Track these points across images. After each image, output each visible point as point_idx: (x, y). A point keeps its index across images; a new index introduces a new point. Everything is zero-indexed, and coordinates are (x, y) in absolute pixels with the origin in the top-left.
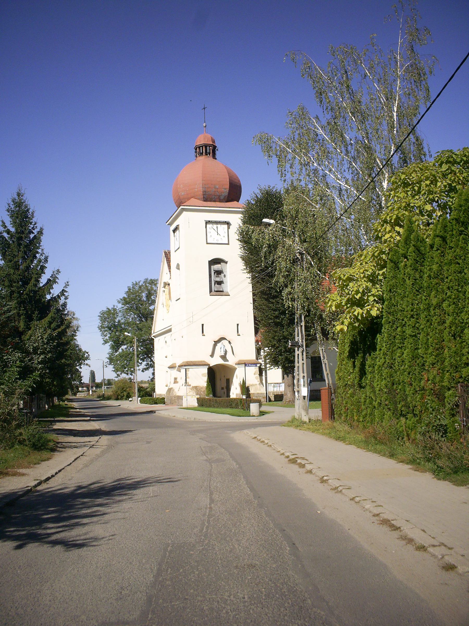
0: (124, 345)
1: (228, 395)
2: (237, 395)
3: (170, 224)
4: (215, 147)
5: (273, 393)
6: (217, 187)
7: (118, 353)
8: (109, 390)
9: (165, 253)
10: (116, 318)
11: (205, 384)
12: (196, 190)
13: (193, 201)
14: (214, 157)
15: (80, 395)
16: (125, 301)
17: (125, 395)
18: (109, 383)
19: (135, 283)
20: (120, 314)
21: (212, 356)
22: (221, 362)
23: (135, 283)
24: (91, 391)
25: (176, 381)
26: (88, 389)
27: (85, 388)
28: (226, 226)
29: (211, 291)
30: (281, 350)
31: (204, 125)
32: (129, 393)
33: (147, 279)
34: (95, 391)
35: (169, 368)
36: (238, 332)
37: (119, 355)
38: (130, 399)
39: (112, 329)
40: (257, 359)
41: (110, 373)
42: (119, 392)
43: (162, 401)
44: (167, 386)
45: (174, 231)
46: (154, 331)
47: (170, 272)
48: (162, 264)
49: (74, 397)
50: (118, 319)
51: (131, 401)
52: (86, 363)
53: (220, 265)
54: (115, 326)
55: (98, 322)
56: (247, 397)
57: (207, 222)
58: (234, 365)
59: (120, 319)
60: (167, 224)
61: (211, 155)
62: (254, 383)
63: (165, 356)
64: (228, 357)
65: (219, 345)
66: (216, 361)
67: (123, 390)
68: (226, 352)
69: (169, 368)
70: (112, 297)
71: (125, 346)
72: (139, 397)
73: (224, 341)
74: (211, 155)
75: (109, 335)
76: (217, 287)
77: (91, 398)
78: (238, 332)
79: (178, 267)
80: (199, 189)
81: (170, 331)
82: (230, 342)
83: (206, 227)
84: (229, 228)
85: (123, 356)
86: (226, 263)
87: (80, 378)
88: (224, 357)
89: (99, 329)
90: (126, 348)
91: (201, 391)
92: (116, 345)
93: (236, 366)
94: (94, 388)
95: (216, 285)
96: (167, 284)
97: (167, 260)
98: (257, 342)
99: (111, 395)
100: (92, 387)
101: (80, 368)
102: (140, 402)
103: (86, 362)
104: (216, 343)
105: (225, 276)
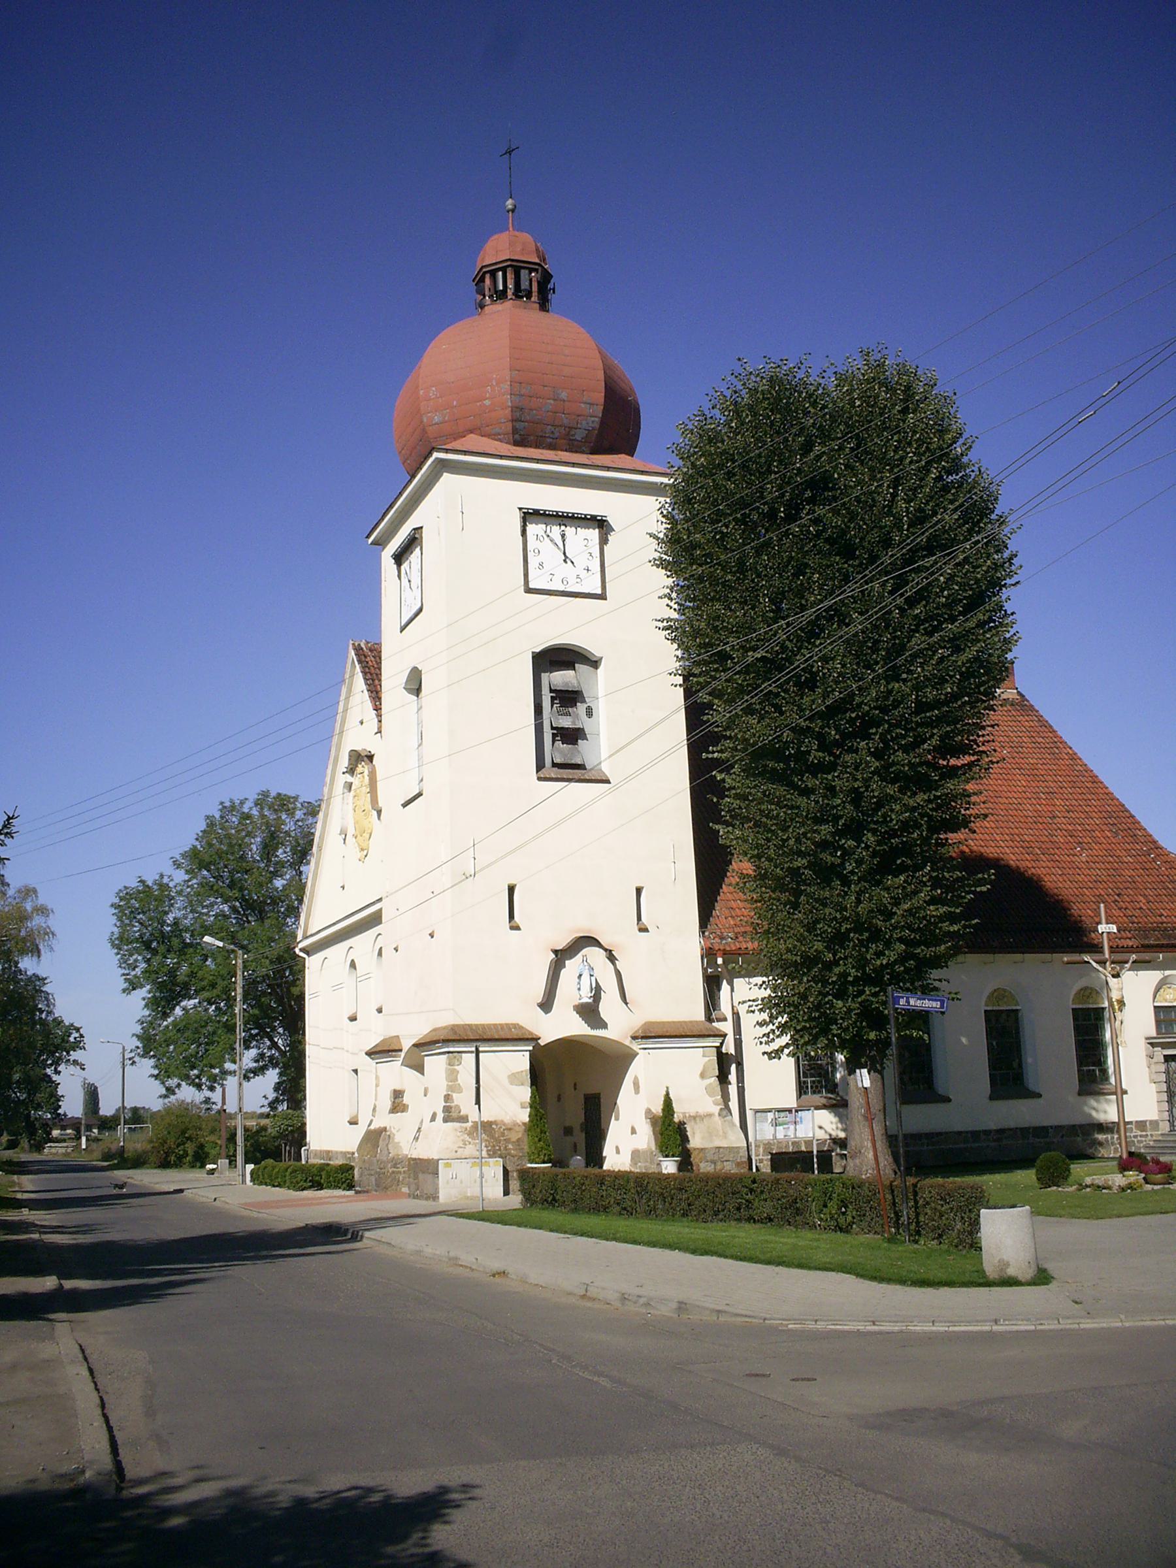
0: (190, 998)
1: (595, 1156)
2: (636, 1154)
3: (381, 543)
4: (546, 277)
5: (768, 1145)
6: (564, 395)
7: (170, 1020)
8: (136, 1136)
9: (358, 650)
10: (166, 913)
11: (524, 1116)
12: (487, 402)
13: (473, 441)
14: (544, 305)
15: (53, 1150)
16: (196, 860)
17: (190, 1152)
18: (137, 1116)
19: (227, 804)
20: (180, 902)
21: (546, 1005)
22: (577, 1027)
23: (227, 804)
24: (84, 1139)
25: (398, 1103)
26: (78, 1131)
27: (69, 1131)
28: (594, 534)
29: (540, 766)
30: (844, 975)
31: (509, 203)
32: (201, 1146)
33: (265, 794)
34: (97, 1140)
35: (370, 1054)
36: (639, 918)
37: (174, 1024)
38: (210, 1166)
39: (154, 944)
40: (709, 1018)
41: (142, 1089)
42: (171, 1142)
43: (338, 1176)
44: (353, 1122)
45: (399, 558)
46: (305, 931)
47: (378, 709)
48: (344, 690)
49: (35, 1157)
50: (171, 917)
51: (212, 1172)
52: (72, 1058)
53: (572, 672)
54: (163, 937)
55: (109, 924)
56: (680, 1169)
57: (530, 516)
58: (627, 1042)
59: (179, 914)
60: (370, 541)
61: (534, 298)
62: (701, 1111)
63: (350, 1014)
64: (604, 1010)
65: (572, 966)
66: (561, 1024)
67: (184, 1135)
68: (597, 992)
69: (370, 1054)
70: (157, 847)
71: (192, 1002)
72: (247, 1161)
73: (591, 952)
74: (534, 298)
75: (144, 965)
76: (561, 752)
77: (83, 1159)
78: (639, 918)
79: (415, 684)
80: (497, 399)
81: (375, 920)
82: (612, 958)
83: (524, 532)
84: (604, 541)
85: (186, 1028)
86: (595, 664)
87: (54, 1100)
88: (590, 1012)
89: (113, 946)
90: (195, 1007)
91: (508, 1141)
92: (167, 994)
93: (635, 1046)
94: (95, 1131)
95: (559, 744)
96: (360, 758)
97: (364, 673)
98: (709, 954)
99: (145, 1152)
100: (89, 1128)
101: (57, 1072)
102: (253, 1180)
103: (74, 1055)
104: (562, 956)
105: (589, 712)
